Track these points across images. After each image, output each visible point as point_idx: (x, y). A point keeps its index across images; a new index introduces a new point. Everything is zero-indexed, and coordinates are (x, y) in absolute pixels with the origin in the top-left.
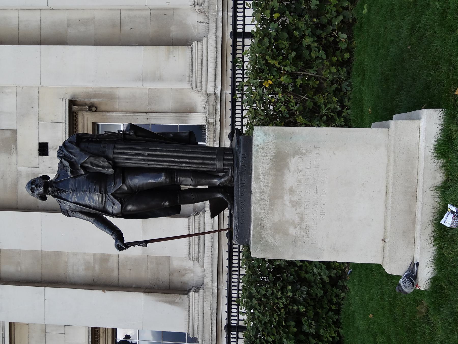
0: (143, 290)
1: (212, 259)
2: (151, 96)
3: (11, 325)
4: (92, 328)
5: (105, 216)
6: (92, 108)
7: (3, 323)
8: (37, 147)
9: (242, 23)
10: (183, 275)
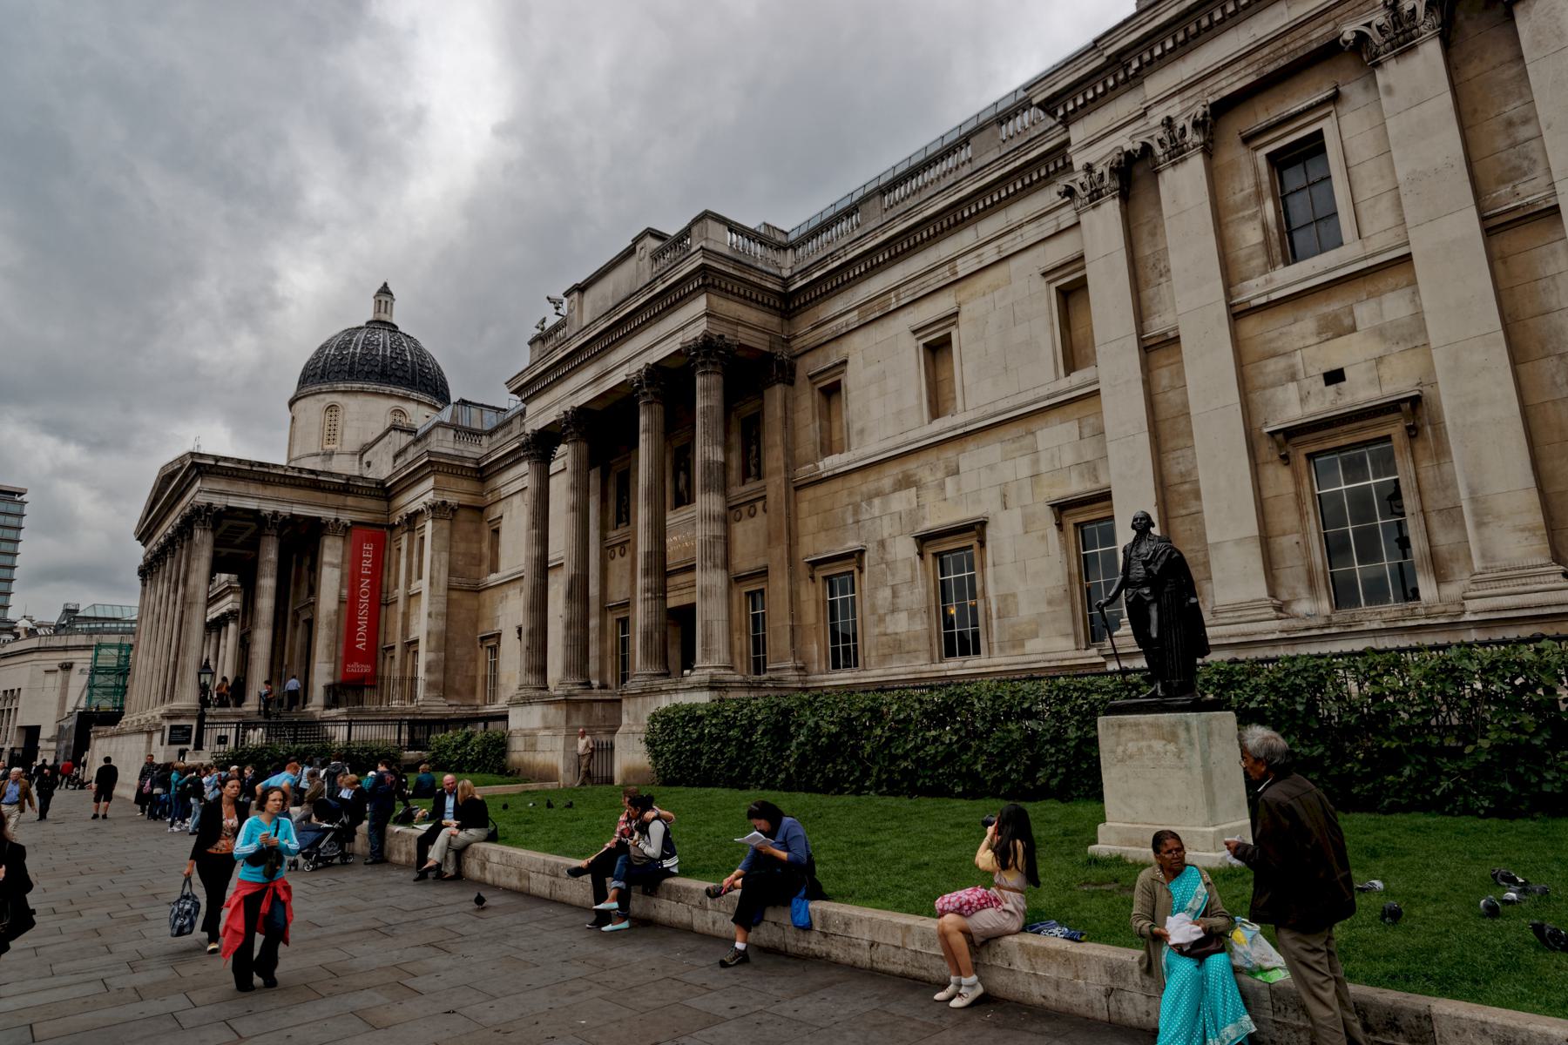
2: (1453, 514)
4: (1557, 206)
5: (256, 954)
6: (1413, 432)
8: (1335, 367)
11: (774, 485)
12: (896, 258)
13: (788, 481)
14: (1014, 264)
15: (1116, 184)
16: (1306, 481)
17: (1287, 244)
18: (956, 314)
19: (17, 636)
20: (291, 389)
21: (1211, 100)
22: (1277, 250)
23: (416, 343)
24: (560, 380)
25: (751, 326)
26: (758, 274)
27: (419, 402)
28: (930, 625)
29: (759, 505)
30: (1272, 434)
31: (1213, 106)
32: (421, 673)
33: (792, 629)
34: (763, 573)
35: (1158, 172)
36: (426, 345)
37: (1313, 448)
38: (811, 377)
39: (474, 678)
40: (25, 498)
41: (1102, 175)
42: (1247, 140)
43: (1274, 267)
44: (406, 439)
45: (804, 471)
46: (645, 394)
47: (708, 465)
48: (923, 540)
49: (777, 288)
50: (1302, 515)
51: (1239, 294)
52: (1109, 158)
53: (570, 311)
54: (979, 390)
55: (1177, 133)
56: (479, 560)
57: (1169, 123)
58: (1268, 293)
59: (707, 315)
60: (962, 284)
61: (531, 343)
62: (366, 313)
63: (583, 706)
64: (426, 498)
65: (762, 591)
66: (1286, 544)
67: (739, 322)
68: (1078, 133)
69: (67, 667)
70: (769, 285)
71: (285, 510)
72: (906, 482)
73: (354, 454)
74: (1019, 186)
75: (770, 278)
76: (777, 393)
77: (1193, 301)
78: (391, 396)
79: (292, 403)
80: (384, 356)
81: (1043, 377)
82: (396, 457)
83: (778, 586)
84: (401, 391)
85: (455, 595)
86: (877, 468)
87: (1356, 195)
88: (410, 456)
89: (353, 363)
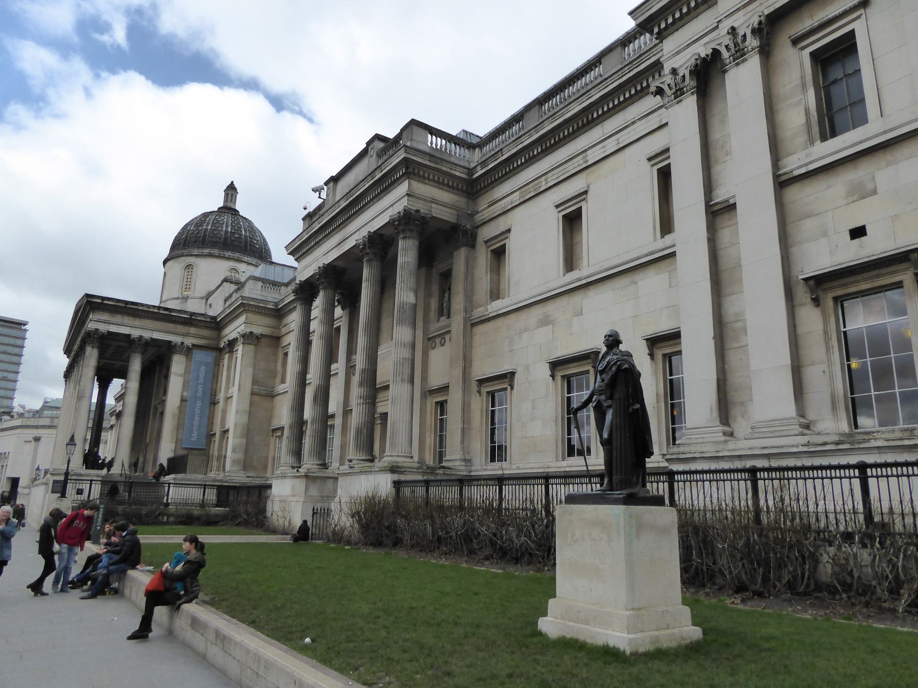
0: (721, 377)
1: (751, 449)
3: (673, 254)
7: (674, 245)
9: (852, 475)
10: (742, 416)
11: (457, 322)
12: (547, 151)
13: (466, 320)
14: (628, 151)
15: (694, 83)
16: (833, 320)
17: (829, 123)
18: (586, 192)
19: (12, 417)
20: (166, 253)
21: (766, 12)
22: (816, 129)
23: (250, 222)
24: (318, 244)
25: (440, 202)
26: (449, 165)
27: (249, 264)
28: (557, 432)
29: (447, 337)
30: (806, 280)
31: (769, 17)
32: (229, 454)
33: (463, 431)
34: (445, 389)
35: (725, 71)
36: (257, 224)
37: (840, 292)
38: (486, 242)
39: (267, 458)
40: (26, 327)
41: (684, 76)
42: (795, 42)
43: (812, 143)
44: (233, 287)
45: (478, 313)
46: (367, 254)
47: (402, 306)
48: (555, 365)
49: (464, 176)
50: (828, 348)
51: (785, 167)
52: (689, 64)
53: (327, 195)
54: (601, 248)
55: (739, 40)
56: (273, 375)
57: (733, 31)
58: (806, 165)
59: (408, 195)
60: (592, 169)
61: (303, 219)
62: (216, 202)
63: (318, 481)
64: (239, 330)
65: (446, 401)
66: (815, 375)
67: (433, 201)
68: (670, 44)
69: (37, 439)
70: (457, 174)
71: (147, 335)
72: (546, 321)
73: (202, 298)
74: (633, 92)
75: (458, 168)
76: (461, 255)
77: (747, 176)
78: (229, 259)
79: (165, 263)
80: (227, 231)
81: (644, 239)
82: (226, 300)
83: (455, 399)
84: (237, 255)
85: (256, 398)
86: (527, 310)
87: (879, 82)
88: (233, 299)
89: (205, 236)
